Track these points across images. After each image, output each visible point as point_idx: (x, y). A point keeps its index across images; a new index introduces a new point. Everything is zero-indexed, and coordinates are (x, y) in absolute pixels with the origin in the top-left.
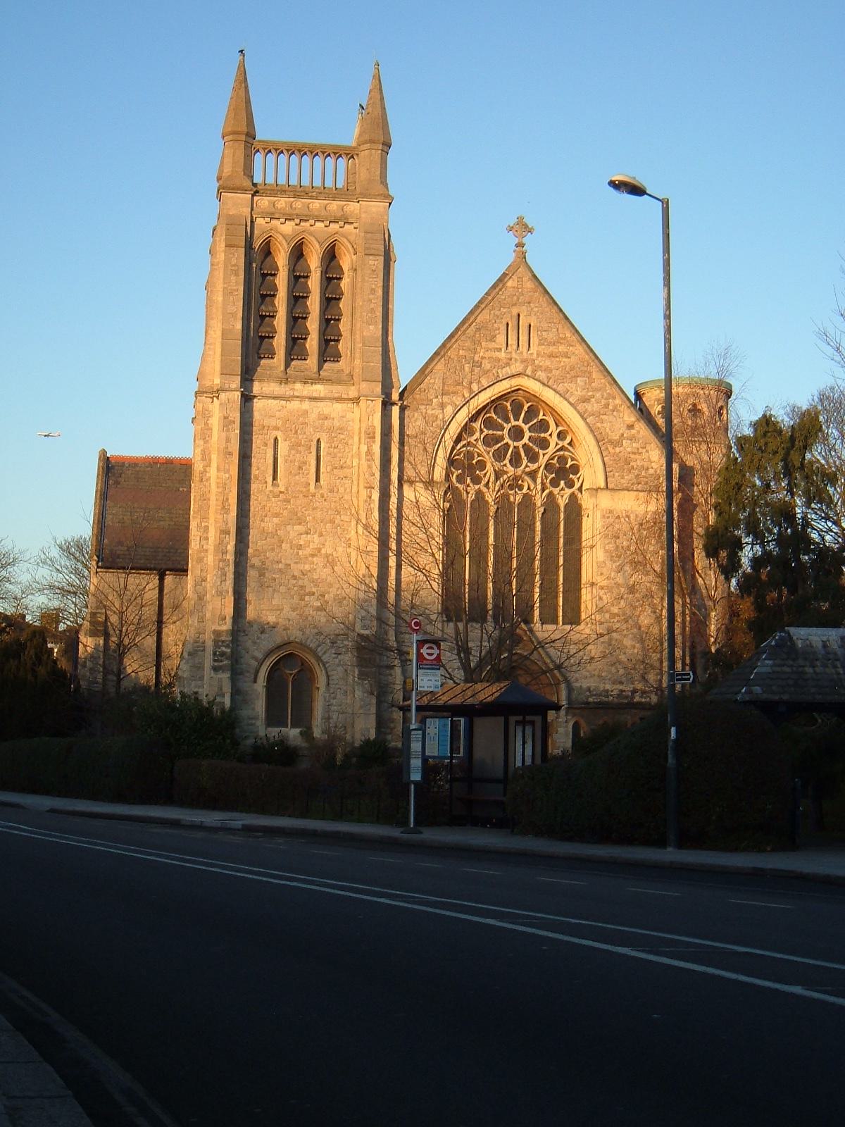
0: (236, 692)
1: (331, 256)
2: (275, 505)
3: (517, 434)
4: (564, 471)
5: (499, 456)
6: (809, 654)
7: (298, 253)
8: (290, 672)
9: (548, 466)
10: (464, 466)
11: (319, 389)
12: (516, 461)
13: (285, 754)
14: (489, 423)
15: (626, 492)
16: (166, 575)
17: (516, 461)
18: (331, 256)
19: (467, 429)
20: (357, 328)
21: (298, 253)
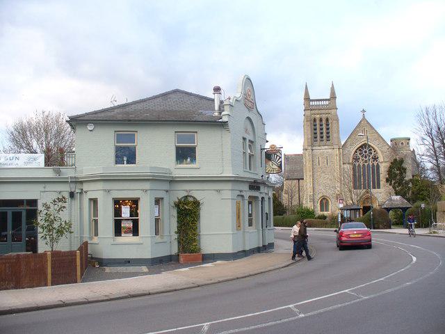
0: (314, 206)
1: (327, 120)
2: (319, 170)
3: (366, 152)
4: (375, 158)
5: (362, 156)
6: (394, 201)
7: (321, 120)
8: (324, 201)
9: (372, 158)
10: (356, 159)
11: (326, 147)
12: (366, 157)
13: (324, 217)
14: (360, 150)
15: (247, 249)
16: (300, 204)
17: (366, 157)
18: (327, 120)
19: (356, 152)
20: (333, 135)
21: (321, 120)
